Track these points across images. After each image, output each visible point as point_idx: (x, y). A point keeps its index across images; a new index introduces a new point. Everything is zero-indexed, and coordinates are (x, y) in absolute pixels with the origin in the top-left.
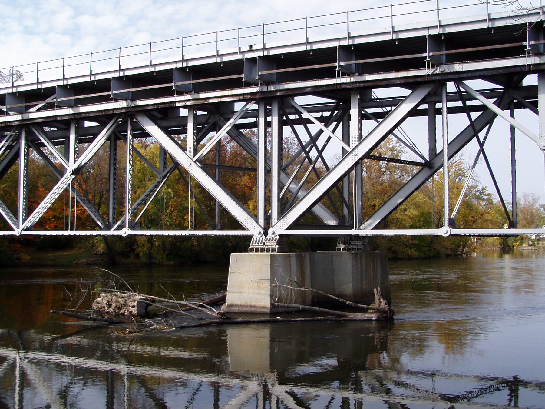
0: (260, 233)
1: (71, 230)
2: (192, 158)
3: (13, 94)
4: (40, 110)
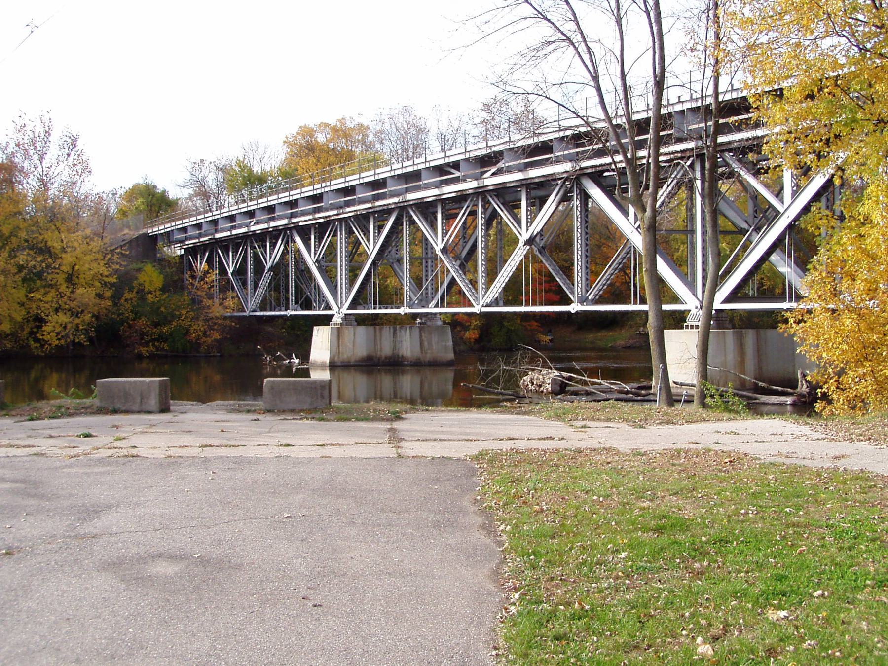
0: (696, 308)
1: (526, 306)
2: (633, 224)
3: (467, 160)
4: (494, 174)
